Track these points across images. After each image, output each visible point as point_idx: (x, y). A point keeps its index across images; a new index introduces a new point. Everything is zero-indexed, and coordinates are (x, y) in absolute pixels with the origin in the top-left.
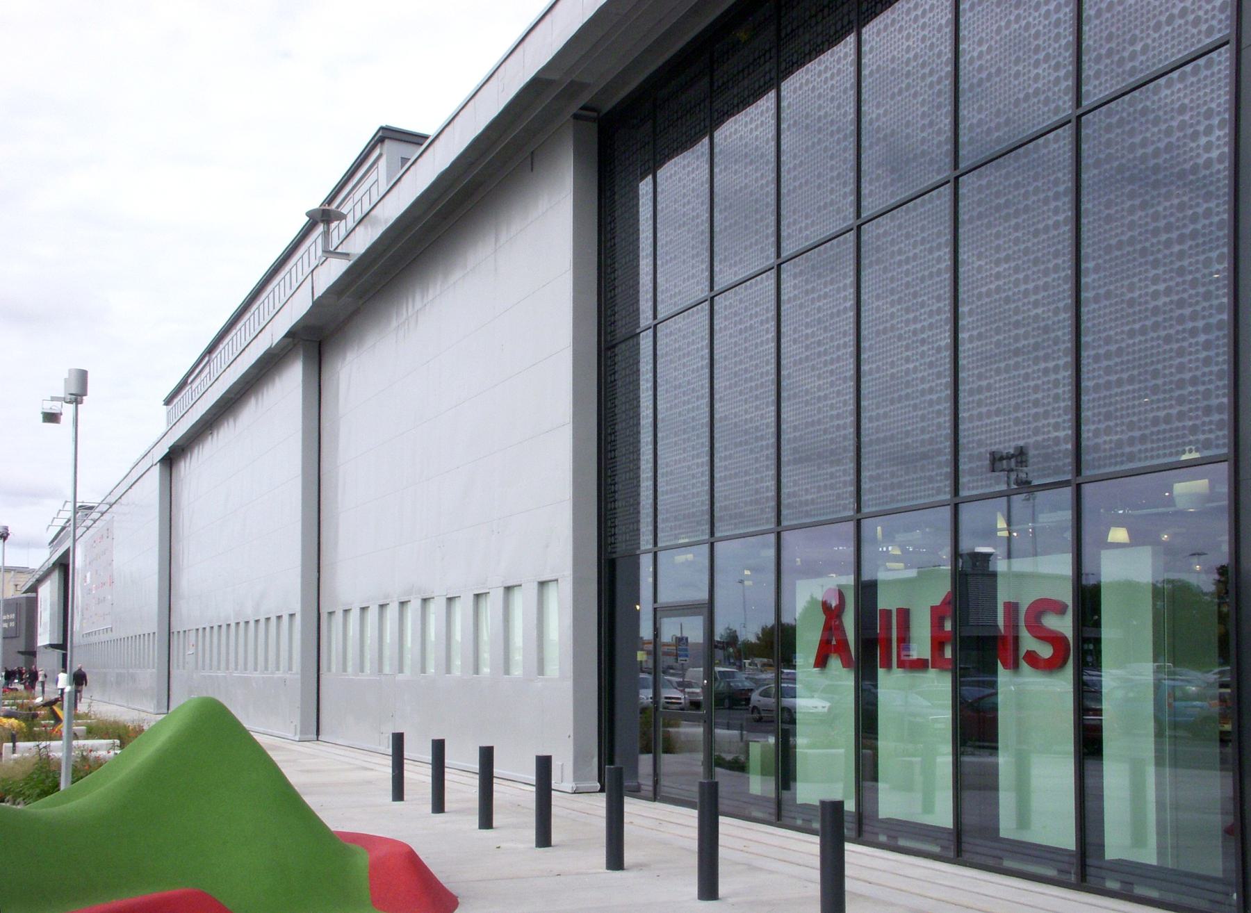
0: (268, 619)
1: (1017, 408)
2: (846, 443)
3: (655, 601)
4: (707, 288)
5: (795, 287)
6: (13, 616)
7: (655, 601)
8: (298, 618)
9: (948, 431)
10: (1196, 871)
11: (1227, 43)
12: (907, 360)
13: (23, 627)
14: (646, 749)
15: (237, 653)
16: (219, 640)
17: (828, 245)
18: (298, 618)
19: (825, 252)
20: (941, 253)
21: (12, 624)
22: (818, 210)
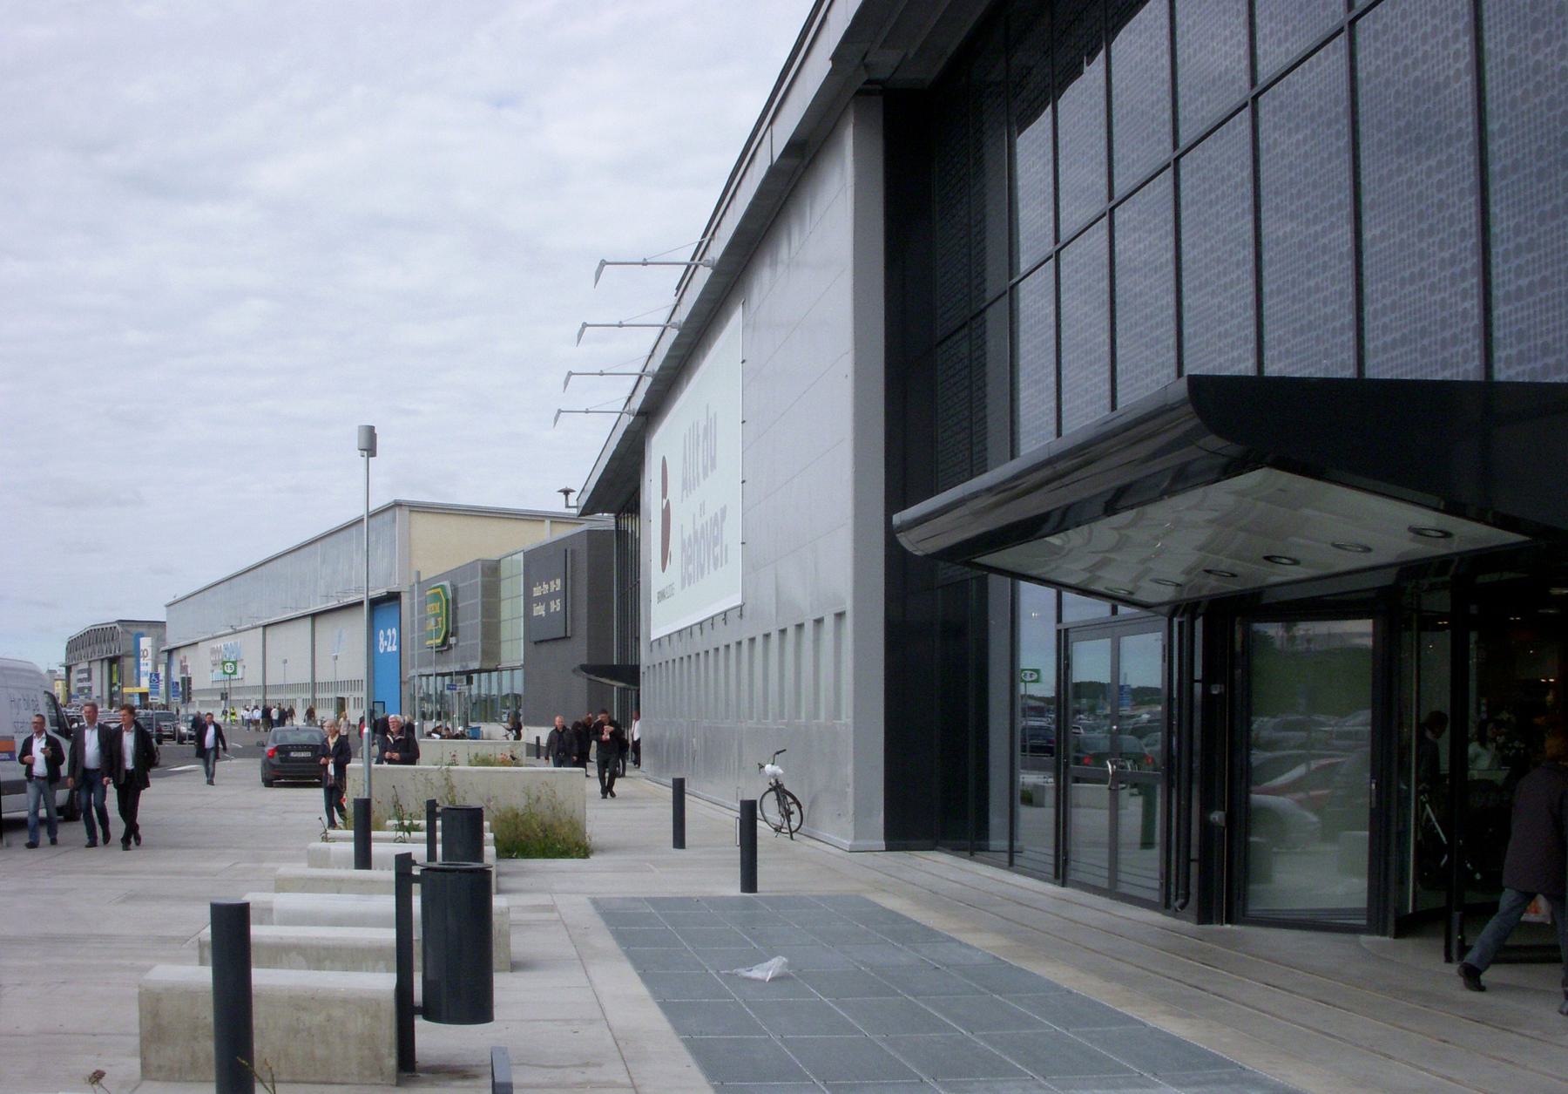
0: (728, 647)
1: (1423, 332)
2: (1345, 356)
3: (1059, 620)
4: (1170, 147)
5: (1378, 53)
6: (557, 585)
7: (1059, 620)
8: (849, 621)
9: (1475, 321)
10: (364, 649)
11: (1245, 105)
12: (1309, 274)
13: (583, 611)
14: (517, 697)
15: (727, 684)
16: (727, 667)
17: (1313, 58)
18: (849, 621)
19: (1319, 64)
20: (1459, 46)
21: (556, 606)
22: (1142, 150)
